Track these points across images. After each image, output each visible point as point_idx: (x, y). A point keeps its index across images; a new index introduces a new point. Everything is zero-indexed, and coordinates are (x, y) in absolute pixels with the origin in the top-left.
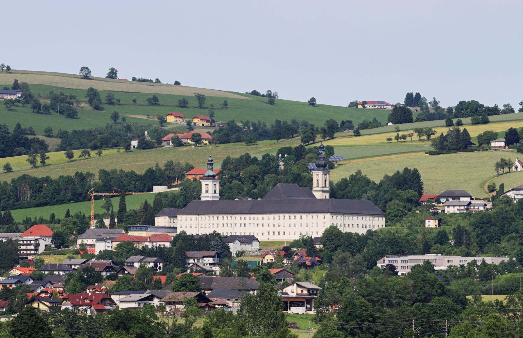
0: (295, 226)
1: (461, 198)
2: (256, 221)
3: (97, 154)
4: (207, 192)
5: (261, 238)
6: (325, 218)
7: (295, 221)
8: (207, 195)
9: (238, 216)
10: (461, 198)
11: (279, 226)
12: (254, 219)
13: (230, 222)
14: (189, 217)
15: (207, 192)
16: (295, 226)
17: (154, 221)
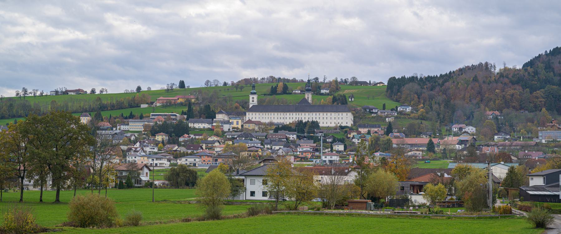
4: (253, 101)
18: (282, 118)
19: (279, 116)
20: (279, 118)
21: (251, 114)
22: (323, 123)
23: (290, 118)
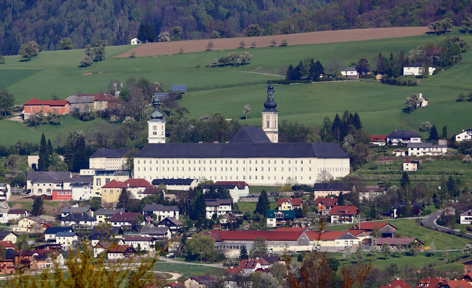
0: (231, 170)
1: (412, 139)
4: (155, 133)
5: (248, 182)
6: (302, 163)
7: (183, 165)
8: (155, 136)
10: (412, 139)
11: (227, 170)
12: (226, 163)
13: (197, 165)
14: (148, 160)
15: (155, 133)
16: (231, 170)
17: (88, 163)
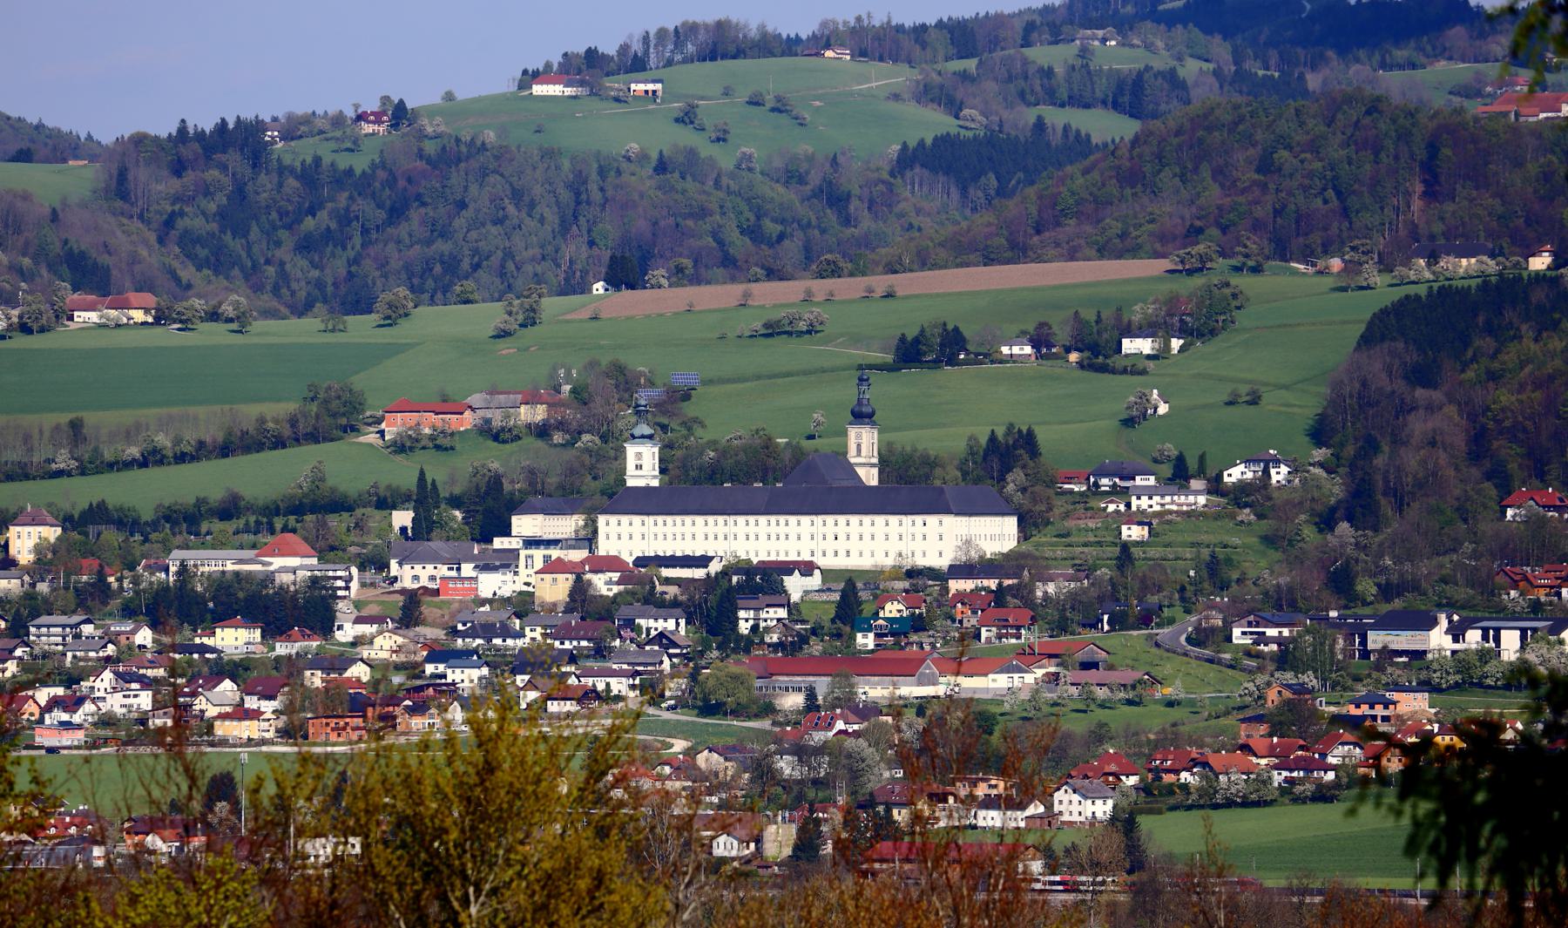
1: (1138, 478)
2: (782, 530)
3: (1400, 508)
4: (639, 467)
8: (639, 473)
9: (741, 519)
10: (1138, 478)
16: (694, 538)
17: (509, 525)
18: (721, 537)
19: (711, 529)
20: (711, 537)
21: (613, 519)
22: (836, 555)
23: (769, 537)
